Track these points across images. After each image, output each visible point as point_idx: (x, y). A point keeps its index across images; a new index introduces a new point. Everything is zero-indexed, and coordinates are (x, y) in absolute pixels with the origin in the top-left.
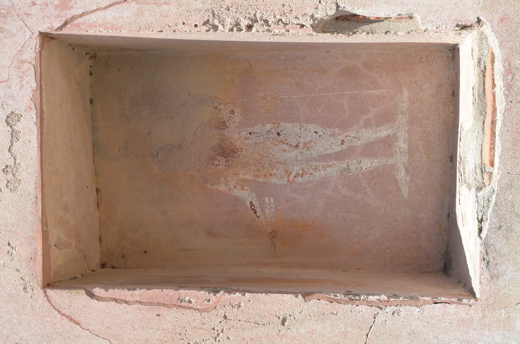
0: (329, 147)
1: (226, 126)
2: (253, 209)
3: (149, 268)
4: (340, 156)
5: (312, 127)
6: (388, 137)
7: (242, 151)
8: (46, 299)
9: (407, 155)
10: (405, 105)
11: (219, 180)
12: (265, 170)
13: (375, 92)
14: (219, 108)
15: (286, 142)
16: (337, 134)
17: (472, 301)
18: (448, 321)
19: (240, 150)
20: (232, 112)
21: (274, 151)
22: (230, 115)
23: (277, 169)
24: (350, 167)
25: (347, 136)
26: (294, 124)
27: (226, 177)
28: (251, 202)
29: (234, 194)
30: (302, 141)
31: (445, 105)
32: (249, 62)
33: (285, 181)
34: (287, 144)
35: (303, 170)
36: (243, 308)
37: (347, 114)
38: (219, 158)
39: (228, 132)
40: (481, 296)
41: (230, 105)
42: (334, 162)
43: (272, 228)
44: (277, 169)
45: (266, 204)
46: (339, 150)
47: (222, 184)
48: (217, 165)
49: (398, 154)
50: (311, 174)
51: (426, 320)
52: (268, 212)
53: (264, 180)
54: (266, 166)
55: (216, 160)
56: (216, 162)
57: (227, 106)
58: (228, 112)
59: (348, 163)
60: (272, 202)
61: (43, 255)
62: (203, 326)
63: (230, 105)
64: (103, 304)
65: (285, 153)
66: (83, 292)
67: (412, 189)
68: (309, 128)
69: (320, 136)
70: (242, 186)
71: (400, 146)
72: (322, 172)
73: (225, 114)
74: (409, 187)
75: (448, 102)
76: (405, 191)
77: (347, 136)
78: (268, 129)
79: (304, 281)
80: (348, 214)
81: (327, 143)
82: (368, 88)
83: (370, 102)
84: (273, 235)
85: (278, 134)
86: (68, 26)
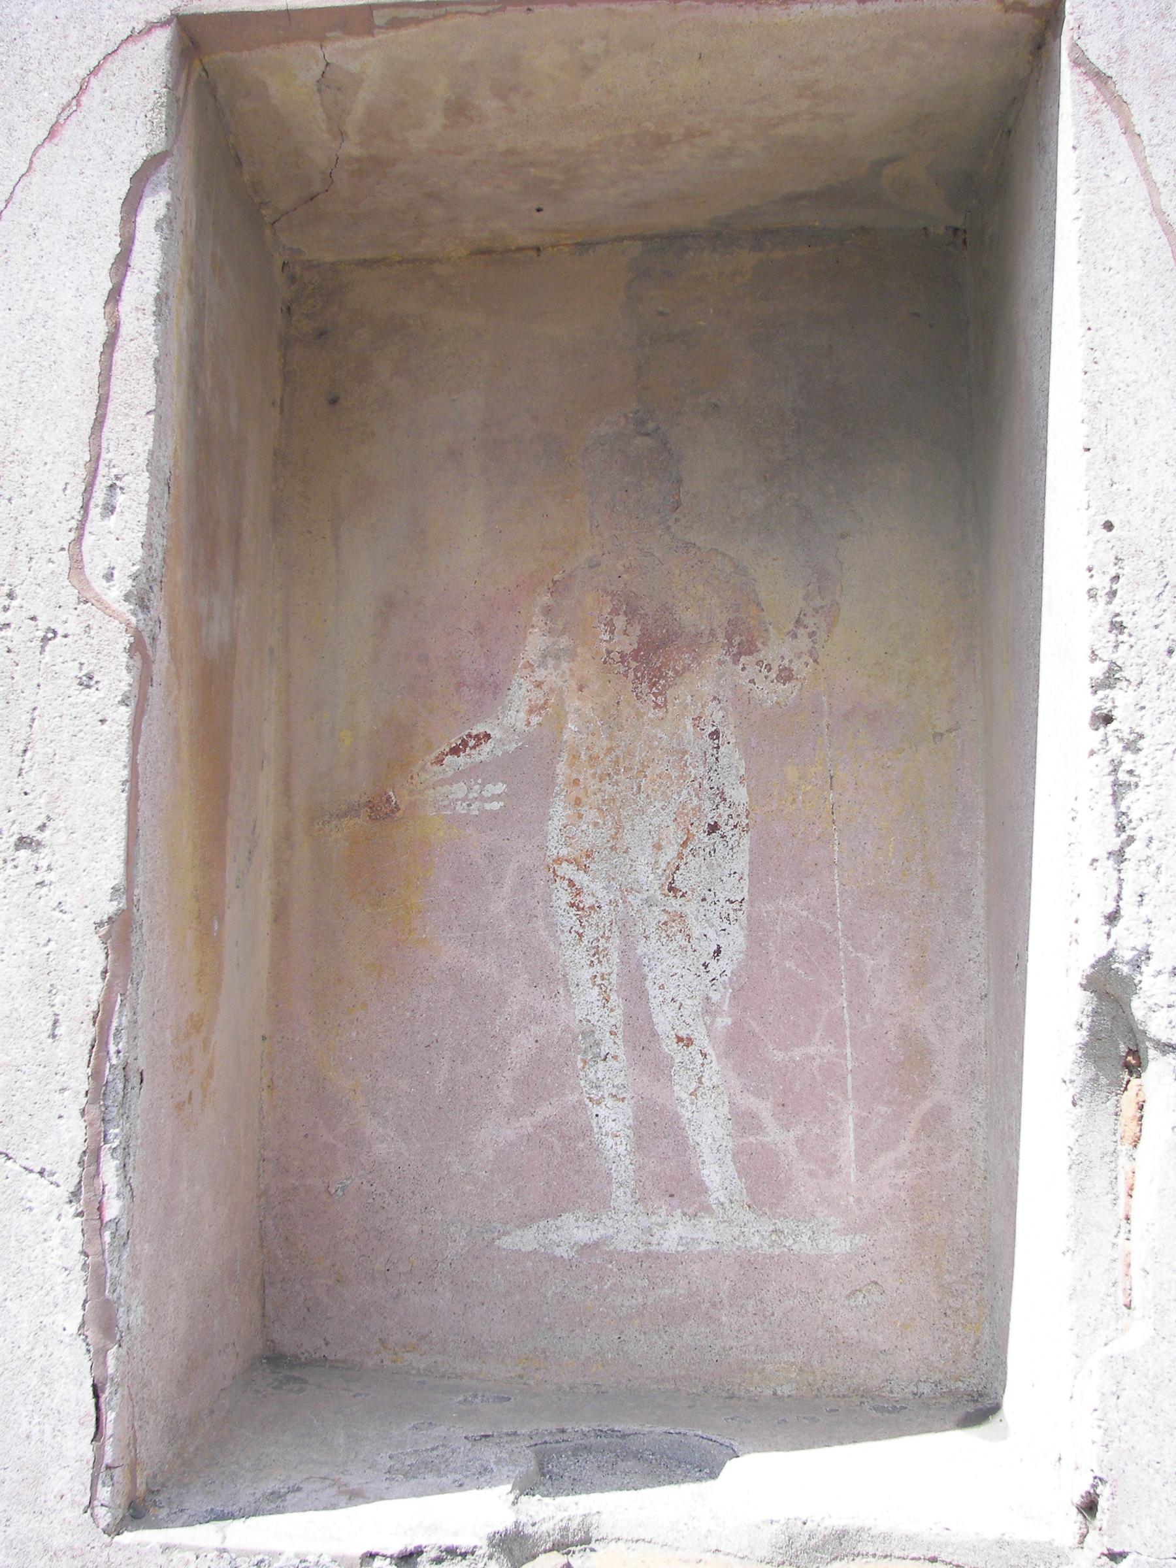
0: (669, 997)
1: (740, 654)
2: (465, 743)
3: (281, 412)
4: (639, 1031)
5: (735, 940)
6: (701, 1188)
7: (657, 706)
8: (139, 27)
9: (642, 1249)
10: (803, 1245)
11: (563, 632)
12: (594, 785)
13: (848, 1146)
14: (801, 632)
15: (686, 852)
16: (713, 1022)
17: (105, 1516)
18: (35, 1430)
19: (660, 699)
20: (786, 676)
21: (656, 813)
22: (775, 669)
23: (596, 824)
24: (601, 1065)
25: (705, 1056)
26: (745, 883)
27: (573, 656)
28: (488, 736)
29: (516, 679)
30: (691, 908)
31: (801, 1369)
32: (949, 731)
33: (556, 847)
34: (680, 856)
35: (592, 907)
36: (82, 698)
37: (779, 1056)
38: (636, 630)
39: (720, 662)
40: (126, 1547)
41: (810, 669)
42: (619, 1011)
43: (402, 807)
44: (596, 824)
45: (483, 785)
46: (660, 1029)
47: (548, 640)
48: (610, 624)
49: (644, 1221)
50: (581, 935)
51: (37, 1353)
52: (455, 796)
53: (560, 779)
54: (609, 788)
55: (629, 622)
56: (620, 622)
57: (806, 658)
58: (786, 662)
59: (615, 1057)
60: (488, 806)
61: (288, 11)
62: (22, 557)
63: (810, 669)
64: (113, 213)
65: (649, 850)
66: (159, 143)
67: (529, 1264)
68: (734, 929)
69: (705, 965)
70: (542, 708)
71: (671, 1225)
72: (586, 974)
73: (778, 650)
74: (535, 1251)
75: (811, 1378)
76: (525, 1240)
77: (705, 1056)
78: (729, 792)
79: (208, 912)
80: (447, 1054)
81: (680, 992)
82: (862, 1124)
83: (816, 1130)
84: (380, 810)
85: (713, 828)
86: (1090, 87)
